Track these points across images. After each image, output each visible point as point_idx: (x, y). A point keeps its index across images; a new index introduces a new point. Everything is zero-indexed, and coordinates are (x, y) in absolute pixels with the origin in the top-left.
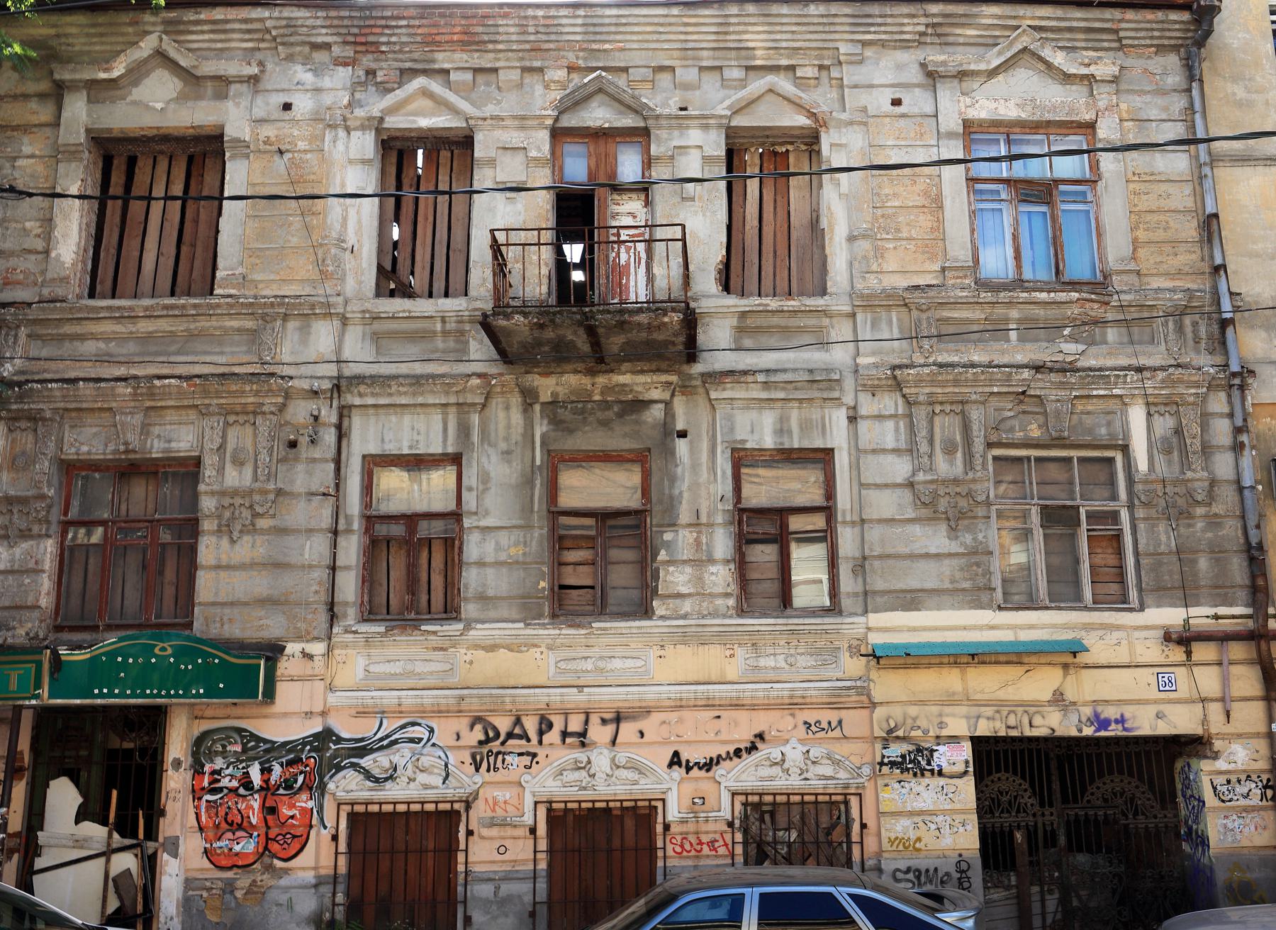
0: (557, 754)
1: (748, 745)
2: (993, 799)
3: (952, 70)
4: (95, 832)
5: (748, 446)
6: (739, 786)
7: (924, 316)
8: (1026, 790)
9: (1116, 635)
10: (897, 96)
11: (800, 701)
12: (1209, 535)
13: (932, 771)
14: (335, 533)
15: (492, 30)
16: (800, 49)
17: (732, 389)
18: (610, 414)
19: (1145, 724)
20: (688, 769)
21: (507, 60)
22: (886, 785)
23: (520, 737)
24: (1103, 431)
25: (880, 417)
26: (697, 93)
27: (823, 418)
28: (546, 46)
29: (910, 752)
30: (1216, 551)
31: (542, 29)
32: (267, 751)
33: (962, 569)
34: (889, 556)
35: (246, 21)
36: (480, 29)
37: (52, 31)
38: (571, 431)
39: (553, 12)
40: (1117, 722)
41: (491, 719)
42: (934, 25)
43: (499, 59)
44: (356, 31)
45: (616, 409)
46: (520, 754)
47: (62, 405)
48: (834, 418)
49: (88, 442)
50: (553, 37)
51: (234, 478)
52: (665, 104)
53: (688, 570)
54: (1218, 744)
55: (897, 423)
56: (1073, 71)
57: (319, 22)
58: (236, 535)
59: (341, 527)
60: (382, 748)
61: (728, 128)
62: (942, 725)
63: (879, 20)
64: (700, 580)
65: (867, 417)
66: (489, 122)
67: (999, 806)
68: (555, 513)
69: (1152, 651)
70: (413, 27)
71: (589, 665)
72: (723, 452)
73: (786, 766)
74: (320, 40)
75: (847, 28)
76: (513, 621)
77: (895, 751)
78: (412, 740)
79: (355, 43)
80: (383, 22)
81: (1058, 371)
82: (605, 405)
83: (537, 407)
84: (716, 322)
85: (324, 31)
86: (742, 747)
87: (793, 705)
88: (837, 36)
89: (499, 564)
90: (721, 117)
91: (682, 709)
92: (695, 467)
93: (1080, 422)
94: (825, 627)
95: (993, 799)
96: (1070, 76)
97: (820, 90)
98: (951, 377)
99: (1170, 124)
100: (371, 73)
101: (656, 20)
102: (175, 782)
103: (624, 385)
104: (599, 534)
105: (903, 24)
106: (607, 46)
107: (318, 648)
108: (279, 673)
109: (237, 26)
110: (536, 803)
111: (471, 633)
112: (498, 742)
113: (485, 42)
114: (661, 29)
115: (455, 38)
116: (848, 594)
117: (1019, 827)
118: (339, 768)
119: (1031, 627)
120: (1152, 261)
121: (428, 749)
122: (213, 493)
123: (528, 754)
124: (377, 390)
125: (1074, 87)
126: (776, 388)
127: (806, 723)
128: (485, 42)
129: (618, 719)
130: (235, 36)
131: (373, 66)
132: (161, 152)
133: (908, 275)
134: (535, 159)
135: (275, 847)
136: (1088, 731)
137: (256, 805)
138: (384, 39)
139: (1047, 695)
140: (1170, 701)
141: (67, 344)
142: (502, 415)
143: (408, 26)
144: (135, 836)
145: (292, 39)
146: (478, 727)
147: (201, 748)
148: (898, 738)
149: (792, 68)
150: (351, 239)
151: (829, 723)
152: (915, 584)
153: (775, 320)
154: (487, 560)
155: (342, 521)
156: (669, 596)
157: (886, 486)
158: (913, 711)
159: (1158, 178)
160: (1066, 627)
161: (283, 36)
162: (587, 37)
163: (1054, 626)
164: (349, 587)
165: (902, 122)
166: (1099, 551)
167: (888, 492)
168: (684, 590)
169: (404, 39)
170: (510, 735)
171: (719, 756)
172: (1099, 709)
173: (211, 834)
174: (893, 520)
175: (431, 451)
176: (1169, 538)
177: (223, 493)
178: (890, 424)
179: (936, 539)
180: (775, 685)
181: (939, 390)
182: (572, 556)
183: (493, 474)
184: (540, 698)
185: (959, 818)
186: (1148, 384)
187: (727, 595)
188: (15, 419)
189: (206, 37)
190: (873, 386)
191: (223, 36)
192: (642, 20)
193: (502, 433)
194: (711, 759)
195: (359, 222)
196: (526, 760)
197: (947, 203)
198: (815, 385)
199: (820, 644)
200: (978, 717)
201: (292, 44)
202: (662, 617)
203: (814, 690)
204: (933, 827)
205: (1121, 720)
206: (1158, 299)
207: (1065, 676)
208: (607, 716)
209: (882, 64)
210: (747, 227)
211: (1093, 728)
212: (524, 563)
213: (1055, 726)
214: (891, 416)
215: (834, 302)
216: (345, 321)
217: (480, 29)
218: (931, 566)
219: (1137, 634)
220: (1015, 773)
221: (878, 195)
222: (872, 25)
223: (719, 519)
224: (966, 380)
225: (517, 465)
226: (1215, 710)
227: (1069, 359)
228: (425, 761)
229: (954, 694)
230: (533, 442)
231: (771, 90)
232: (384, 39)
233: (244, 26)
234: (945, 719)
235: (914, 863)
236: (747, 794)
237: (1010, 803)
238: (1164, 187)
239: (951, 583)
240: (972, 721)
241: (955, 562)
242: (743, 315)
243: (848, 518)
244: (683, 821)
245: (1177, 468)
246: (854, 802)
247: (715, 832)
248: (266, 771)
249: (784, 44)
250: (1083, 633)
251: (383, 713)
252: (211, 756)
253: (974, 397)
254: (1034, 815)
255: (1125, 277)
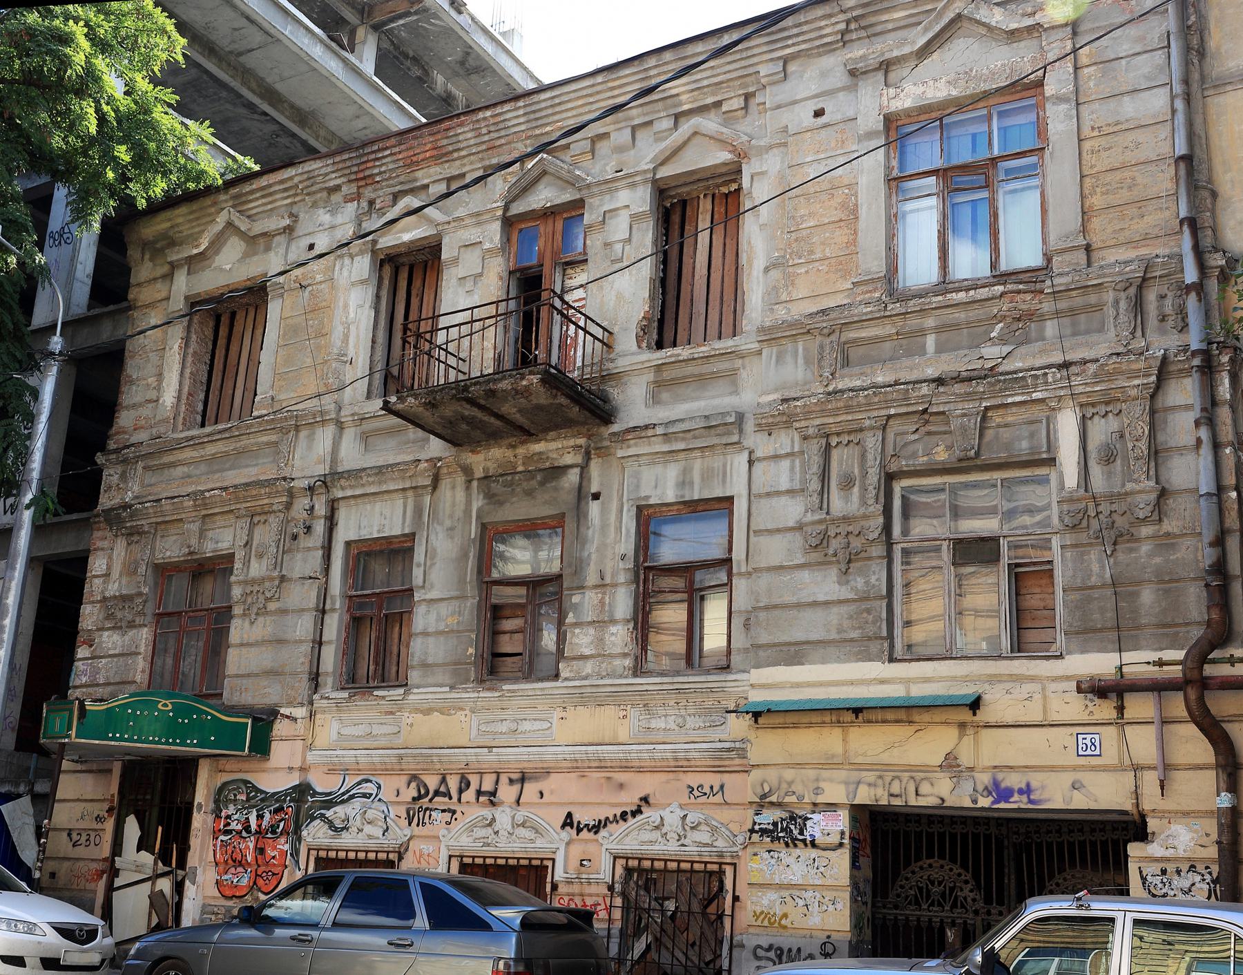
0: (474, 812)
1: (634, 808)
2: (920, 889)
3: (873, 62)
4: (147, 858)
5: (652, 502)
6: (617, 848)
7: (828, 341)
8: (966, 882)
9: (1028, 687)
10: (819, 106)
11: (685, 763)
12: (1158, 560)
13: (804, 841)
14: (324, 612)
15: (454, 140)
16: (722, 83)
17: (636, 445)
18: (534, 483)
19: (1057, 795)
20: (579, 830)
21: (471, 163)
22: (755, 854)
23: (444, 795)
24: (1025, 444)
25: (776, 457)
26: (632, 152)
27: (725, 466)
28: (498, 143)
29: (782, 820)
30: (1168, 582)
31: (492, 128)
32: (257, 798)
33: (851, 617)
34: (775, 607)
35: (282, 182)
36: (445, 142)
37: (168, 225)
38: (501, 503)
39: (498, 110)
40: (1021, 792)
41: (423, 778)
42: (856, 19)
43: (464, 165)
44: (355, 169)
45: (539, 478)
46: (443, 811)
47: (154, 520)
48: (736, 463)
49: (170, 549)
50: (503, 133)
51: (257, 569)
52: (604, 171)
53: (592, 631)
54: (1152, 824)
55: (793, 461)
56: (1014, 26)
57: (329, 169)
59: (328, 607)
60: (343, 802)
61: (655, 182)
62: (818, 791)
63: (795, 31)
64: (601, 640)
65: (765, 459)
66: (453, 224)
67: (928, 897)
68: (486, 583)
69: (1074, 707)
70: (394, 154)
71: (504, 727)
72: (629, 510)
73: (664, 831)
74: (332, 184)
75: (765, 49)
76: (441, 686)
77: (768, 817)
78: (364, 795)
79: (357, 180)
80: (373, 156)
81: (963, 381)
82: (529, 475)
83: (475, 484)
84: (634, 379)
85: (333, 176)
86: (628, 810)
87: (678, 767)
88: (755, 60)
89: (439, 633)
90: (645, 172)
91: (572, 767)
92: (604, 527)
93: (997, 437)
94: (710, 685)
95: (920, 889)
96: (1012, 32)
97: (749, 119)
98: (841, 404)
99: (1145, 56)
100: (371, 203)
101: (585, 92)
102: (200, 822)
103: (540, 453)
104: (529, 602)
105: (821, 28)
106: (548, 129)
107: (300, 712)
108: (274, 732)
109: (277, 188)
110: (450, 857)
111: (411, 697)
112: (427, 800)
113: (451, 152)
114: (591, 100)
115: (428, 154)
116: (739, 650)
117: (953, 924)
118: (313, 819)
119: (927, 680)
120: (1109, 230)
121: (376, 804)
122: (239, 582)
123: (449, 810)
124: (353, 483)
125: (1022, 44)
126: (676, 440)
127: (689, 787)
128: (451, 152)
129: (523, 780)
130: (278, 196)
131: (373, 196)
132: (248, 304)
133: (818, 299)
134: (489, 250)
135: (260, 882)
136: (985, 802)
137: (251, 845)
138: (376, 171)
139: (938, 759)
140: (1094, 769)
141: (166, 471)
142: (448, 494)
143: (391, 154)
144: (170, 865)
145: (314, 189)
146: (413, 785)
147: (220, 798)
148: (772, 804)
149: (718, 104)
150: (351, 352)
151: (712, 787)
152: (799, 636)
153: (690, 369)
154: (430, 630)
155: (328, 601)
156: (574, 659)
157: (778, 530)
158: (789, 774)
159: (1124, 127)
160: (966, 679)
161: (308, 187)
162: (530, 125)
163: (954, 679)
164: (329, 658)
165: (823, 132)
166: (1037, 590)
167: (778, 537)
168: (587, 652)
169: (391, 166)
170: (437, 793)
171: (607, 818)
172: (1000, 776)
173: (221, 868)
174: (781, 567)
175: (394, 533)
176: (1103, 567)
177: (246, 582)
178: (786, 464)
179: (825, 585)
180: (658, 747)
181: (831, 420)
182: (508, 625)
183: (439, 551)
184: (461, 756)
185: (829, 895)
186: (1076, 381)
187: (625, 655)
188: (131, 534)
189: (260, 202)
190: (768, 425)
191: (270, 199)
192: (573, 96)
193: (448, 512)
194: (600, 821)
195: (358, 336)
196: (448, 816)
197: (863, 212)
198: (713, 431)
199: (708, 704)
200: (859, 783)
201: (314, 193)
202: (566, 679)
203: (696, 752)
204: (801, 903)
205: (1027, 791)
206: (1104, 276)
207: (960, 738)
208: (515, 776)
209: (806, 76)
210: (697, 277)
211: (991, 799)
212: (458, 632)
213: (945, 795)
214: (787, 455)
215: (743, 341)
216: (340, 426)
217: (445, 142)
218: (818, 615)
219: (1053, 686)
220: (953, 860)
221: (793, 217)
222: (789, 37)
223: (622, 578)
224: (859, 405)
225: (458, 540)
226: (1150, 780)
227: (989, 365)
228: (371, 814)
229: (833, 756)
230: (471, 516)
231: (696, 133)
232: (376, 171)
233: (282, 187)
234: (822, 785)
235: (777, 941)
236: (627, 859)
237: (943, 895)
238: (1131, 136)
239: (838, 633)
240: (852, 787)
241: (844, 609)
242: (659, 368)
243: (743, 569)
244: (569, 882)
245: (1118, 480)
246: (729, 870)
247: (598, 895)
248: (260, 817)
249: (705, 83)
250: (987, 686)
251: (346, 772)
252: (227, 802)
253: (867, 423)
254: (976, 912)
255: (1067, 257)
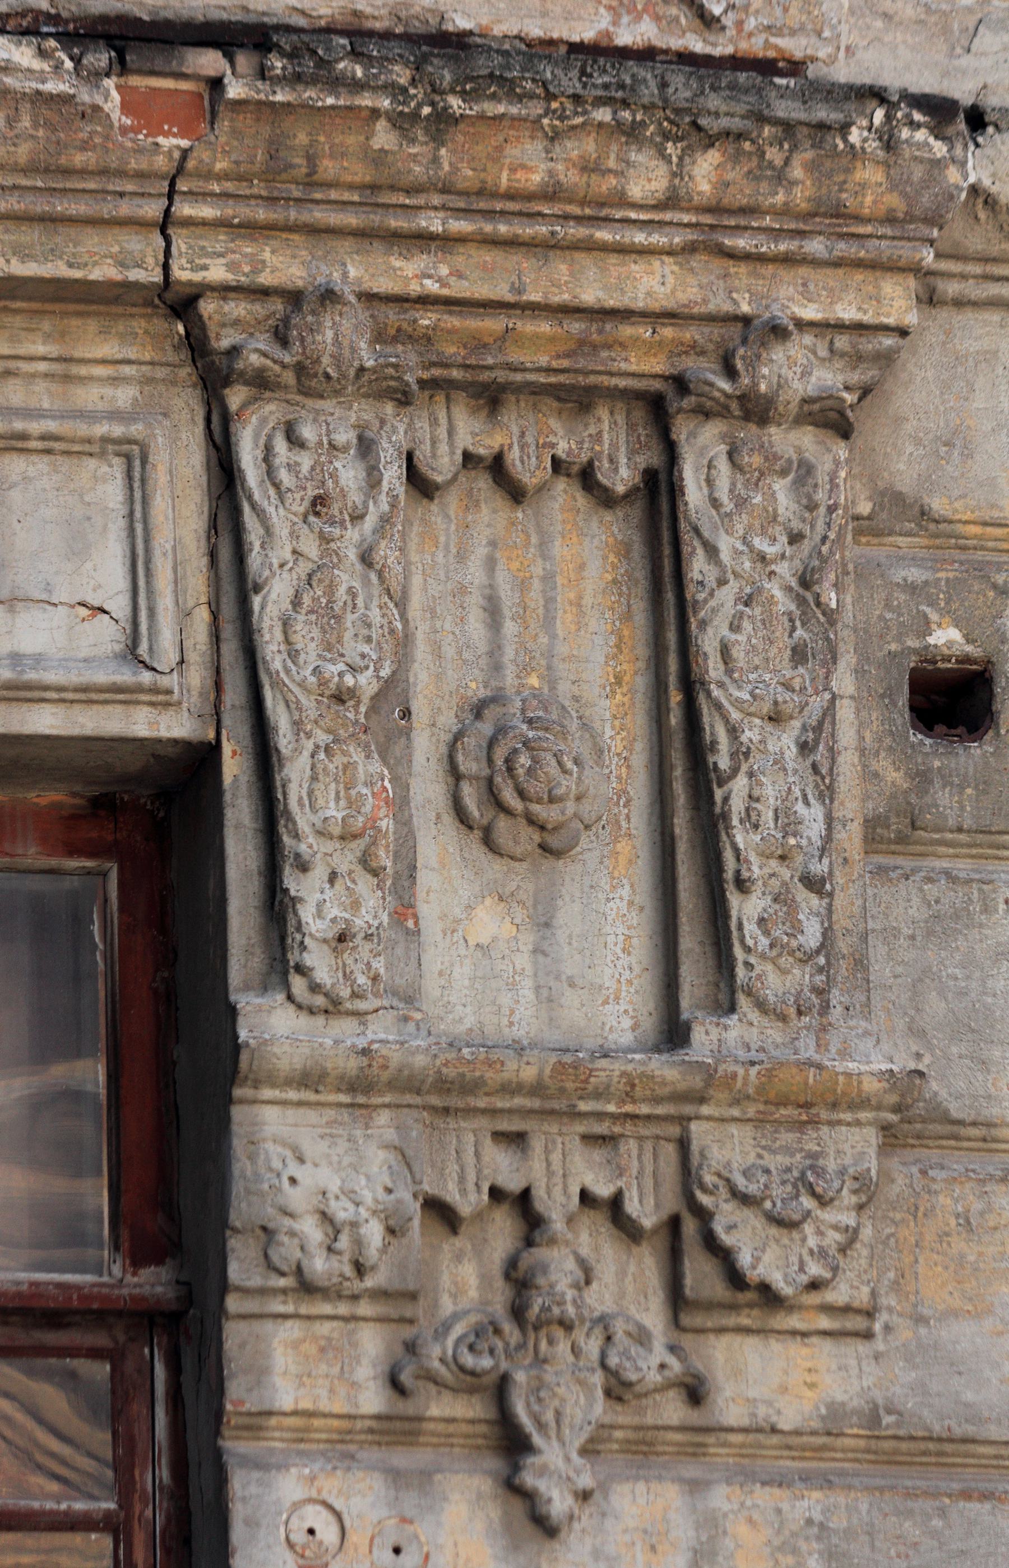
58: (556, 1469)
122: (361, 1088)
177: (446, 1093)
